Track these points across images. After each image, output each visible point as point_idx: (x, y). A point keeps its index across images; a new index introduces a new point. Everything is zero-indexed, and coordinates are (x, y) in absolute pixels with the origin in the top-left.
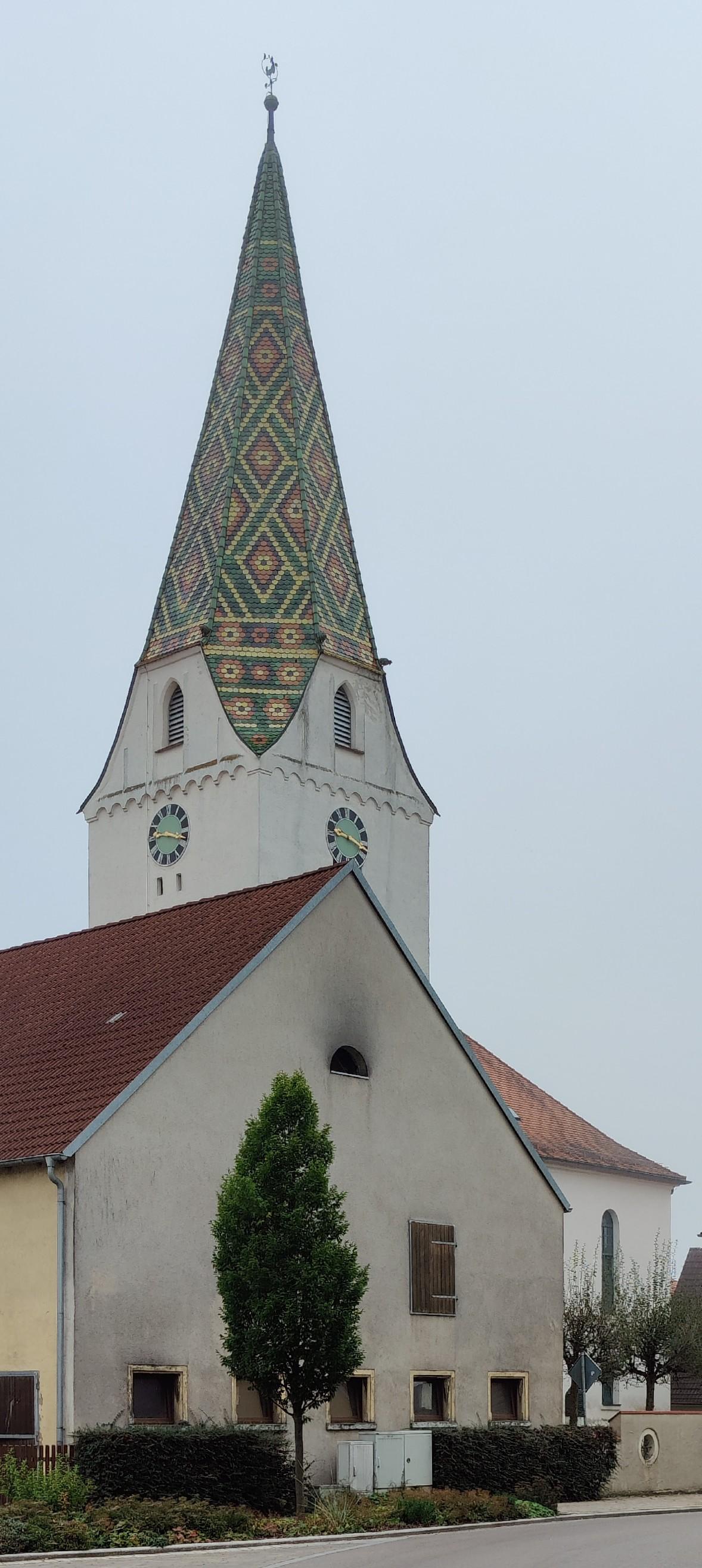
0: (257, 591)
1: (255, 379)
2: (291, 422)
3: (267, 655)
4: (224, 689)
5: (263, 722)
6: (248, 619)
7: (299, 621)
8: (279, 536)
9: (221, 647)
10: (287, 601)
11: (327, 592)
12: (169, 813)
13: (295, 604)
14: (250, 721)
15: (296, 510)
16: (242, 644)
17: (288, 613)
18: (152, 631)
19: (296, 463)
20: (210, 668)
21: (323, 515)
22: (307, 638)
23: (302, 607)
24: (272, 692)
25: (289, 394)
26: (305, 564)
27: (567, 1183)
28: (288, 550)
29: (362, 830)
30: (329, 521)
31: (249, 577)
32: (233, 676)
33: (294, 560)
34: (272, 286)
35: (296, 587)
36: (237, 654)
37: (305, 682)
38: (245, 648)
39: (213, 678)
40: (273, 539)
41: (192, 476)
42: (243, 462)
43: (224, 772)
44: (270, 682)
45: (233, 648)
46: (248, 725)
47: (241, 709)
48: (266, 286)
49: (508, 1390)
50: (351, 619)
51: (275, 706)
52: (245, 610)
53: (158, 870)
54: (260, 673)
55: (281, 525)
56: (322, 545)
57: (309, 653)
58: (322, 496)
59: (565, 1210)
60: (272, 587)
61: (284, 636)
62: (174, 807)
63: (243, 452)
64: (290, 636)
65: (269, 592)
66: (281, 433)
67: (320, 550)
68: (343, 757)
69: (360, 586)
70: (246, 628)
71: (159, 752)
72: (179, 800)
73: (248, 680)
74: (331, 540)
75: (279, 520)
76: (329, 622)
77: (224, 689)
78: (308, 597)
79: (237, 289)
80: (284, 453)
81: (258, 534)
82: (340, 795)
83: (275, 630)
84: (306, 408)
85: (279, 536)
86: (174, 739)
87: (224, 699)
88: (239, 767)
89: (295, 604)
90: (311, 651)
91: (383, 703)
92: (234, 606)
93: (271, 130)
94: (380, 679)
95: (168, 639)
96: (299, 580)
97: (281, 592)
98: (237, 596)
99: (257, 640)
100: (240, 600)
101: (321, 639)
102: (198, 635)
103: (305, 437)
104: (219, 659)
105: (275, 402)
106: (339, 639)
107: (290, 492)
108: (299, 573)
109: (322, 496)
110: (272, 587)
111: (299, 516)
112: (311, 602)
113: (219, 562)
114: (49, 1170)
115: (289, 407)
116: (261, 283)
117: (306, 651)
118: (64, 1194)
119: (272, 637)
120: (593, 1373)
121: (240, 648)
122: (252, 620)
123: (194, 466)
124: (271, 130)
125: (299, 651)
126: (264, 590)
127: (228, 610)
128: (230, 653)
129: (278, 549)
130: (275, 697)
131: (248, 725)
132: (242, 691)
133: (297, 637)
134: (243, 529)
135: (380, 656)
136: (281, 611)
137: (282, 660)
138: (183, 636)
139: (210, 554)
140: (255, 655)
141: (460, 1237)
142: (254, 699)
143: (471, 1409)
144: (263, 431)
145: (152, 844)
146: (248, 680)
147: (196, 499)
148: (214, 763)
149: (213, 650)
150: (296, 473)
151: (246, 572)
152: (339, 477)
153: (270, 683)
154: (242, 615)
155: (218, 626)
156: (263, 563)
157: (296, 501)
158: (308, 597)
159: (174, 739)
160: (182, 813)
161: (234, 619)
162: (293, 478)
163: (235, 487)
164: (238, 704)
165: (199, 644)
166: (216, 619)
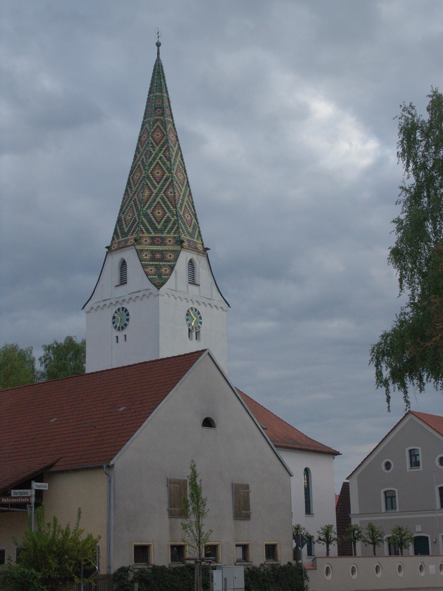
0: (156, 224)
1: (154, 144)
2: (169, 159)
3: (161, 249)
4: (144, 263)
5: (160, 276)
6: (153, 235)
7: (174, 235)
8: (165, 203)
9: (142, 246)
10: (168, 228)
11: (184, 223)
12: (121, 310)
13: (172, 229)
14: (155, 275)
15: (171, 193)
16: (151, 245)
17: (169, 232)
18: (113, 239)
19: (170, 175)
20: (138, 255)
21: (182, 194)
22: (177, 242)
23: (174, 230)
24: (163, 263)
25: (168, 149)
26: (175, 213)
27: (289, 458)
28: (168, 208)
29: (200, 316)
30: (184, 196)
31: (153, 218)
32: (147, 257)
33: (171, 211)
34: (160, 110)
35: (172, 222)
36: (149, 249)
37: (176, 260)
38: (152, 246)
39: (139, 259)
40: (162, 204)
41: (129, 179)
42: (150, 175)
43: (144, 295)
44: (162, 259)
45: (147, 246)
46: (154, 277)
47: (151, 270)
48: (158, 110)
49: (271, 551)
50: (194, 233)
51: (165, 269)
52: (152, 231)
53: (116, 333)
54: (158, 256)
55: (166, 198)
56: (181, 205)
57: (177, 248)
58: (181, 186)
59: (291, 476)
60: (162, 222)
61: (167, 241)
62: (123, 308)
63: (150, 171)
64: (170, 241)
65: (161, 224)
66: (164, 164)
67: (181, 208)
68: (191, 287)
69: (196, 219)
70: (152, 238)
71: (116, 286)
72: (125, 306)
73: (153, 259)
74: (185, 203)
75: (164, 197)
76: (185, 235)
77: (144, 263)
78: (177, 226)
79: (146, 110)
80: (166, 171)
81: (156, 202)
82: (190, 302)
83: (163, 239)
84: (174, 154)
85: (165, 203)
86: (123, 281)
87: (144, 267)
88: (151, 293)
89: (172, 229)
90: (178, 247)
91: (206, 262)
92: (147, 230)
93: (158, 53)
94: (206, 256)
95: (119, 242)
96: (173, 219)
97: (166, 224)
98: (148, 226)
99: (157, 243)
100: (149, 228)
101: (182, 242)
102: (133, 241)
103: (174, 165)
104: (142, 251)
105: (162, 152)
106: (189, 241)
107: (168, 186)
108: (173, 217)
109: (181, 186)
110: (162, 222)
111: (173, 195)
112: (178, 228)
113: (141, 213)
114: (105, 469)
115: (168, 154)
116: (156, 109)
117: (176, 247)
118: (110, 478)
119: (162, 241)
120: (304, 541)
121: (150, 246)
122: (154, 235)
123: (130, 175)
124: (158, 53)
125: (174, 247)
126: (159, 223)
127: (145, 231)
128: (146, 248)
129: (164, 208)
130: (164, 265)
131: (154, 277)
132: (151, 263)
133: (173, 241)
134: (150, 200)
135: (206, 246)
136: (166, 231)
137: (166, 250)
138: (126, 241)
139: (137, 209)
140: (156, 249)
141: (251, 488)
142: (156, 266)
143: (258, 558)
144: (158, 163)
145: (114, 323)
146: (153, 259)
147: (131, 188)
148: (140, 291)
149: (139, 247)
150: (171, 178)
151: (152, 217)
152: (187, 179)
153: (162, 260)
154: (151, 233)
155: (141, 238)
156: (159, 213)
157: (171, 189)
158: (177, 226)
159: (123, 281)
160: (126, 310)
161: (147, 235)
162: (170, 180)
163: (147, 184)
164: (150, 268)
165: (132, 245)
166: (140, 235)
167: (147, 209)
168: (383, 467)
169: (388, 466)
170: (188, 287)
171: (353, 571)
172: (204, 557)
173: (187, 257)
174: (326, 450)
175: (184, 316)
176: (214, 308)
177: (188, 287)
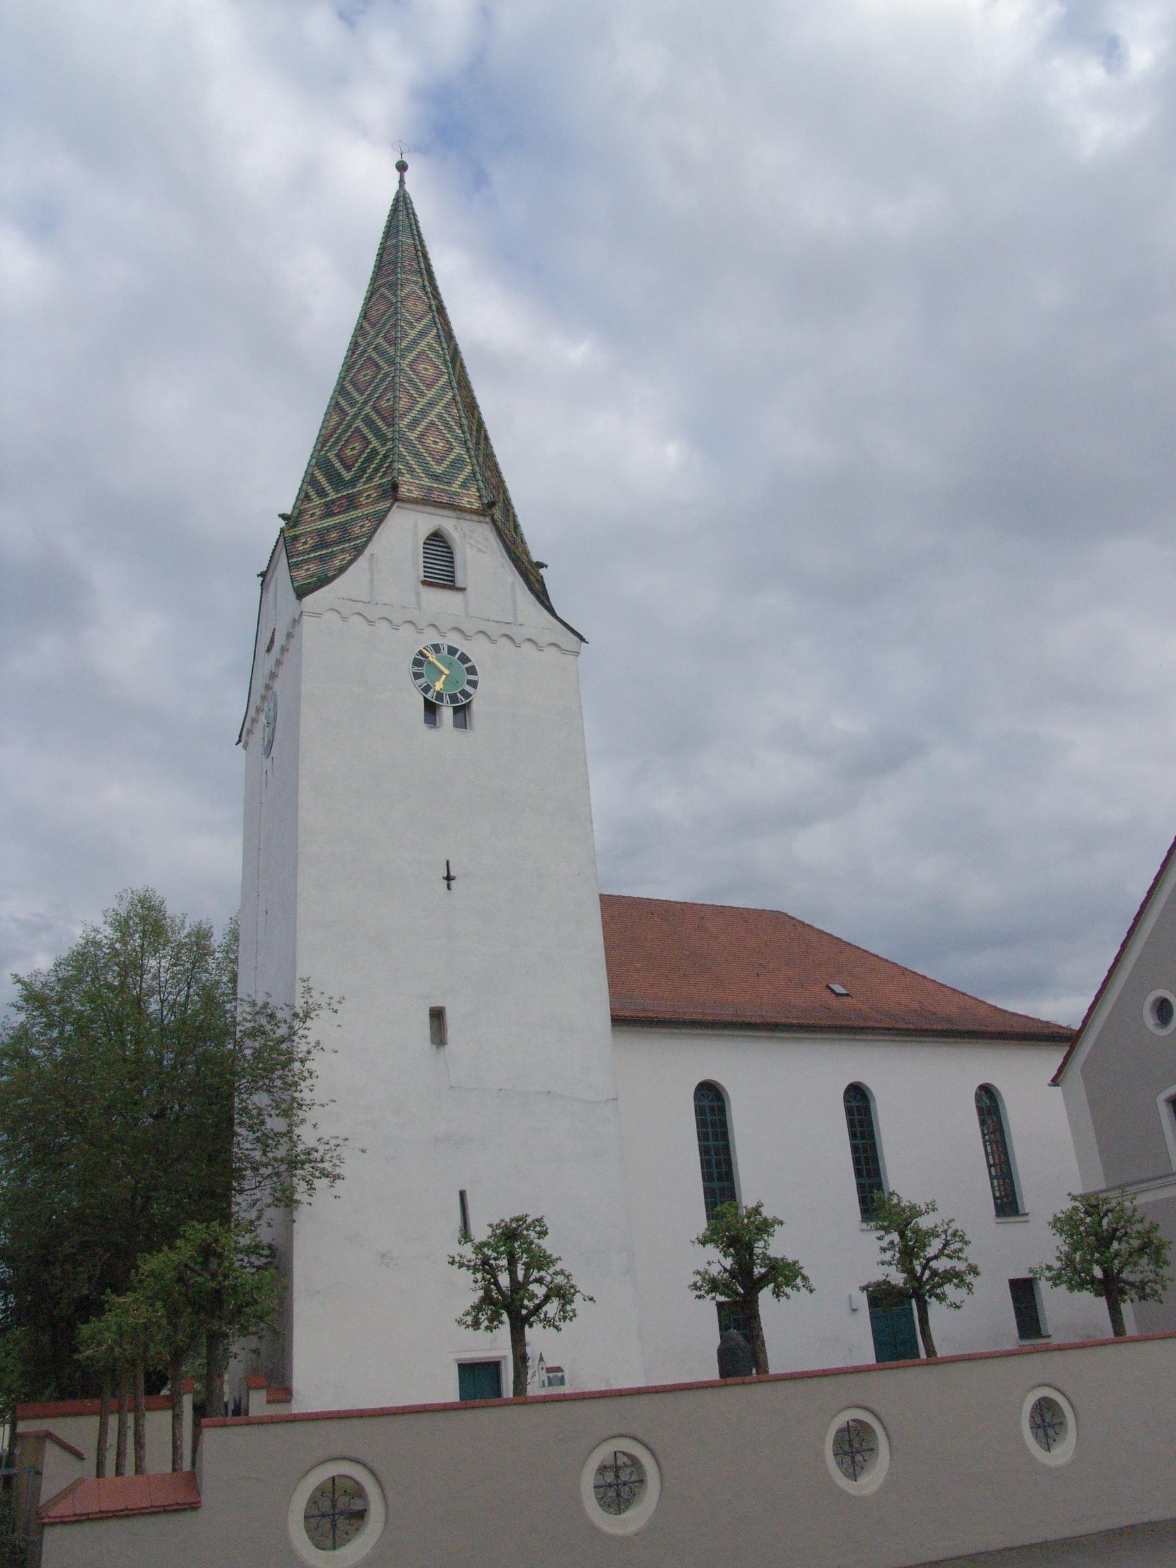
96: (383, 451)
167: (328, 451)
168: (1150, 1020)
169: (1163, 1010)
170: (418, 594)
171: (1047, 1420)
172: (511, 1395)
173: (416, 525)
174: (1018, 1028)
175: (407, 667)
176: (527, 646)
177: (418, 594)
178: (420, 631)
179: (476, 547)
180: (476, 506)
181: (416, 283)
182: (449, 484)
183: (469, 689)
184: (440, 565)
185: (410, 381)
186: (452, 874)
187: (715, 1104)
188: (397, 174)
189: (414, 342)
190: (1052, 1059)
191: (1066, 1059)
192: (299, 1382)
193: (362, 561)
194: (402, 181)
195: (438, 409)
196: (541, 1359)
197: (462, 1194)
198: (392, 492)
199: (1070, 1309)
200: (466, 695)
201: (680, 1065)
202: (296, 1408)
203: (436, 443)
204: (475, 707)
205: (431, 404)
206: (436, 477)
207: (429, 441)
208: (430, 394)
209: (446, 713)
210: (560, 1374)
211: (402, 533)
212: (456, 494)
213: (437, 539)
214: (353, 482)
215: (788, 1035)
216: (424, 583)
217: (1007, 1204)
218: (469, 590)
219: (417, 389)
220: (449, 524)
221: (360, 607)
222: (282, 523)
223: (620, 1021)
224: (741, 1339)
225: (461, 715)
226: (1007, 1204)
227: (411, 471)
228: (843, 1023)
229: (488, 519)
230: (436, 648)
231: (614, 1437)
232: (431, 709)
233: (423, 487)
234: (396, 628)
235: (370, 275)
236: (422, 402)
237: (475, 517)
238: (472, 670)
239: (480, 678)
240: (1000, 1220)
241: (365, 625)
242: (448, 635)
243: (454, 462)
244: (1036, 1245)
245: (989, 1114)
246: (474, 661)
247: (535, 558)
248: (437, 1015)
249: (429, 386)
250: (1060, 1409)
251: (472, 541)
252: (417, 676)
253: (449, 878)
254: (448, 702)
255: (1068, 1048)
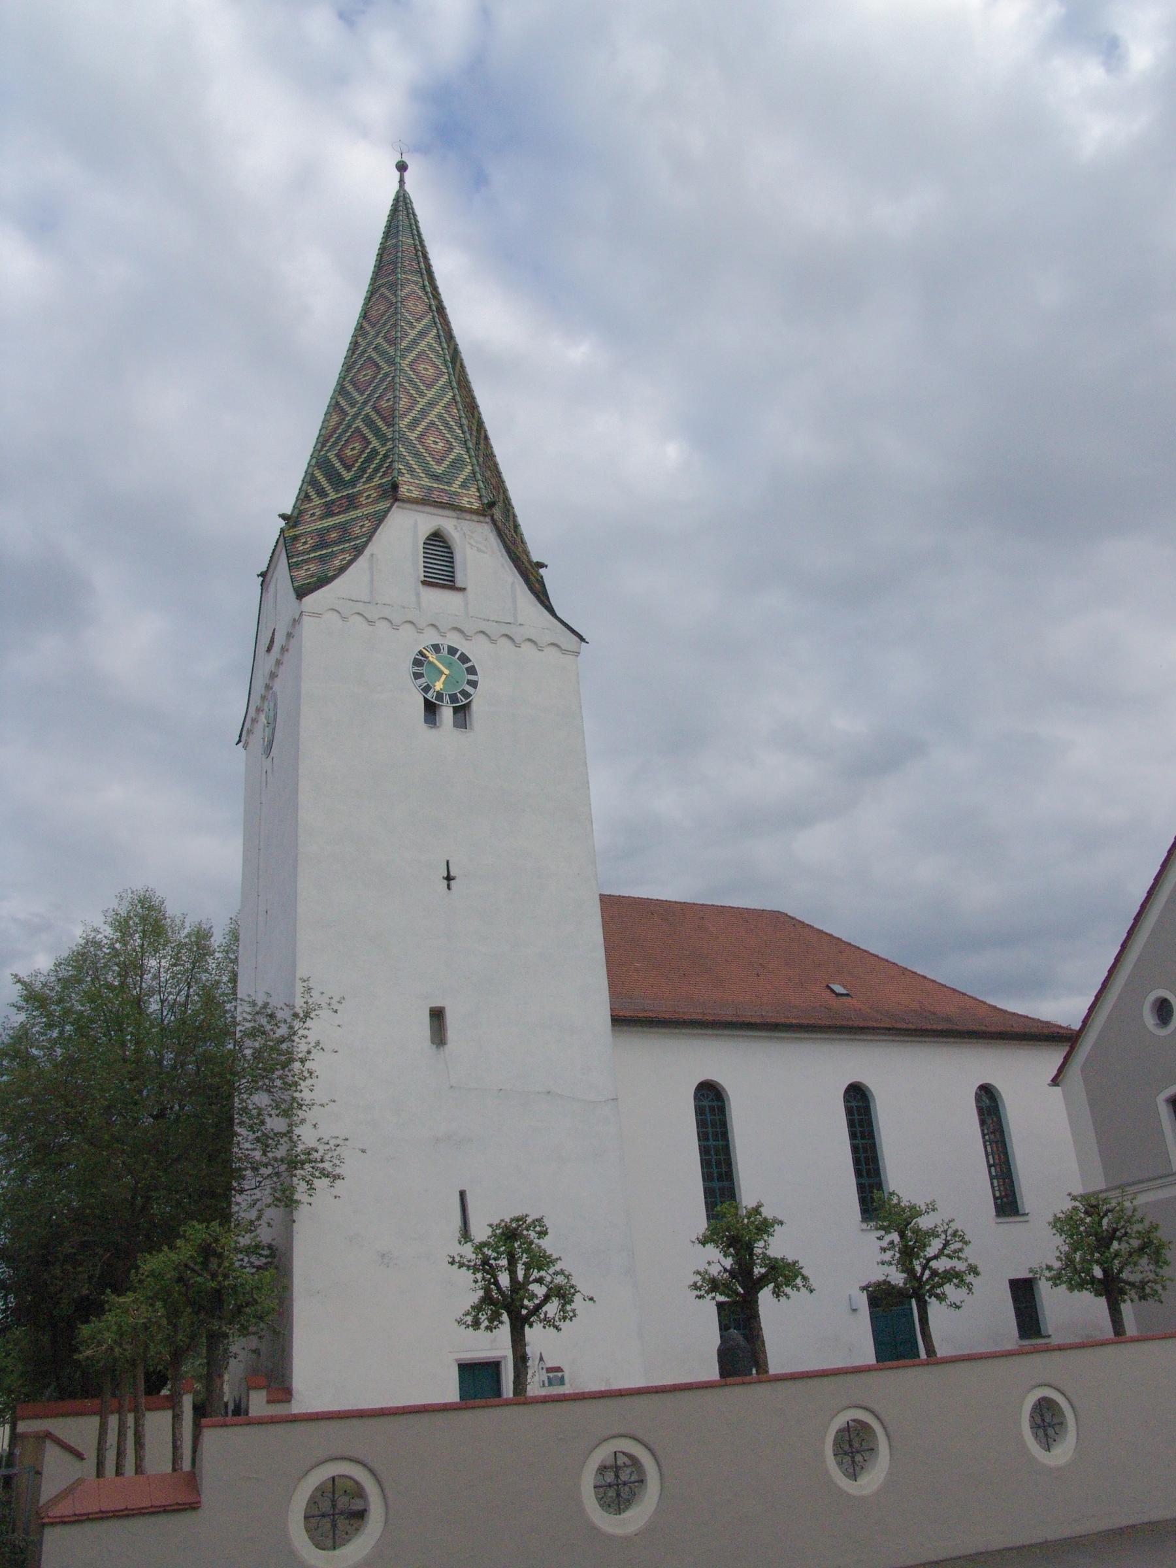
96: (383, 451)
167: (328, 451)
168: (1150, 1020)
169: (1163, 1010)
170: (418, 594)
171: (1047, 1420)
172: (511, 1395)
173: (416, 525)
174: (1018, 1028)
175: (407, 667)
176: (527, 646)
177: (418, 594)
178: (420, 631)
179: (476, 547)
180: (476, 506)
181: (416, 283)
182: (449, 484)
183: (469, 689)
184: (440, 565)
185: (410, 381)
186: (452, 874)
187: (715, 1104)
188: (397, 174)
189: (414, 342)
190: (1052, 1059)
191: (1066, 1059)
192: (299, 1382)
193: (362, 561)
194: (402, 181)
195: (438, 409)
196: (541, 1359)
197: (462, 1194)
198: (392, 492)
199: (1070, 1309)
200: (466, 695)
201: (680, 1065)
202: (296, 1408)
203: (436, 443)
204: (475, 707)
205: (431, 404)
206: (436, 477)
207: (429, 441)
208: (430, 394)
209: (446, 713)
210: (560, 1374)
211: (402, 533)
212: (456, 494)
213: (437, 539)
214: (353, 482)
215: (788, 1035)
216: (424, 583)
217: (1007, 1204)
218: (469, 590)
219: (417, 389)
220: (449, 524)
221: (360, 607)
222: (282, 523)
223: (620, 1021)
224: (741, 1339)
225: (461, 715)
226: (1007, 1204)
227: (411, 471)
228: (843, 1023)
229: (488, 519)
230: (436, 648)
231: (614, 1437)
232: (431, 709)
233: (423, 487)
234: (396, 628)
235: (370, 275)
236: (422, 402)
237: (475, 517)
238: (472, 670)
239: (480, 678)
240: (1000, 1220)
241: (365, 625)
242: (448, 635)
243: (454, 462)
244: (1036, 1245)
245: (989, 1114)
246: (474, 661)
247: (535, 558)
248: (437, 1015)
249: (429, 386)
250: (1060, 1409)
251: (472, 541)
252: (417, 676)
253: (449, 878)
254: (448, 702)
255: (1068, 1048)
